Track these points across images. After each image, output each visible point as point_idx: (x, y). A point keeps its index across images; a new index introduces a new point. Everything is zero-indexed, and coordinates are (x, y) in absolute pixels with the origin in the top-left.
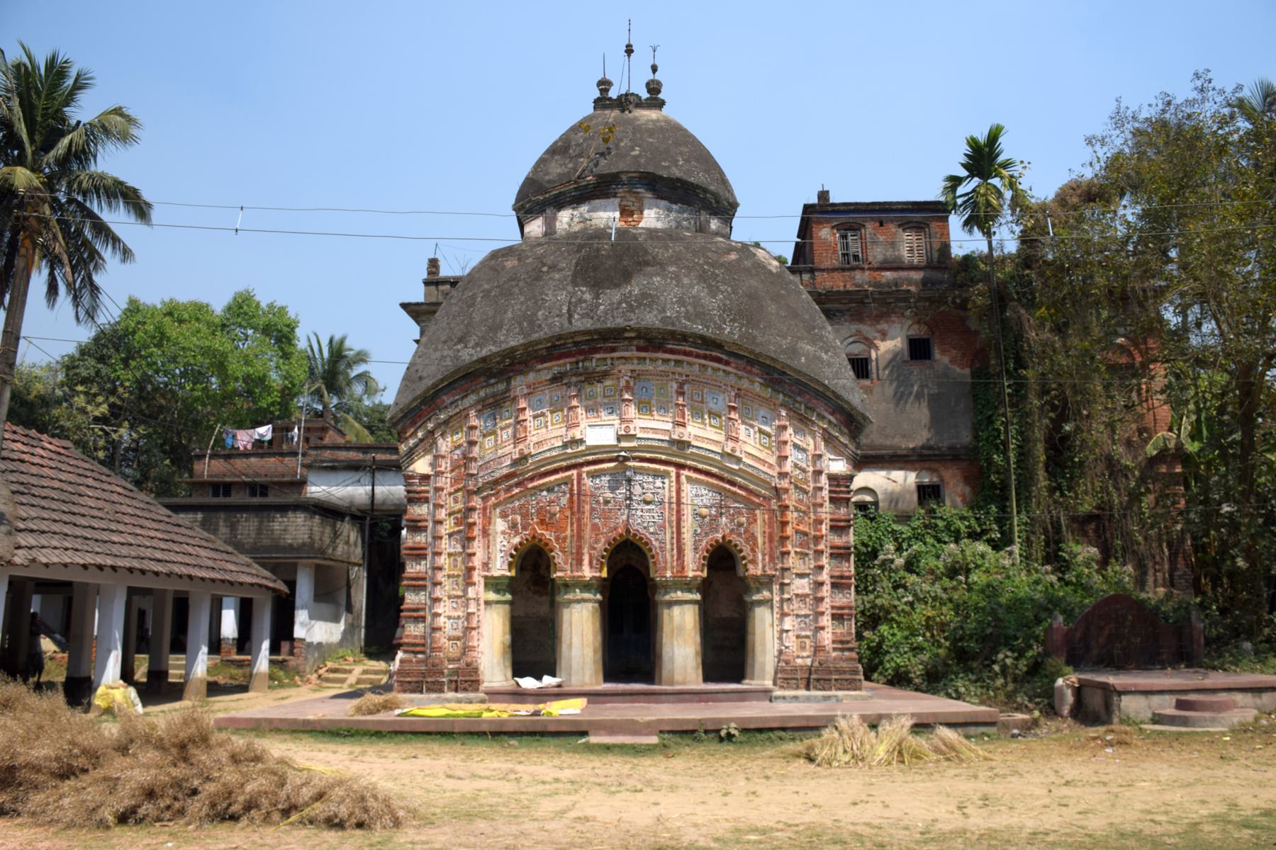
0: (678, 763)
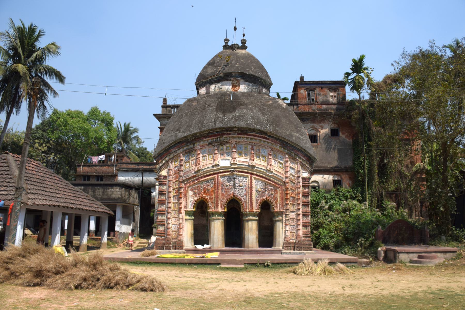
0: (251, 274)
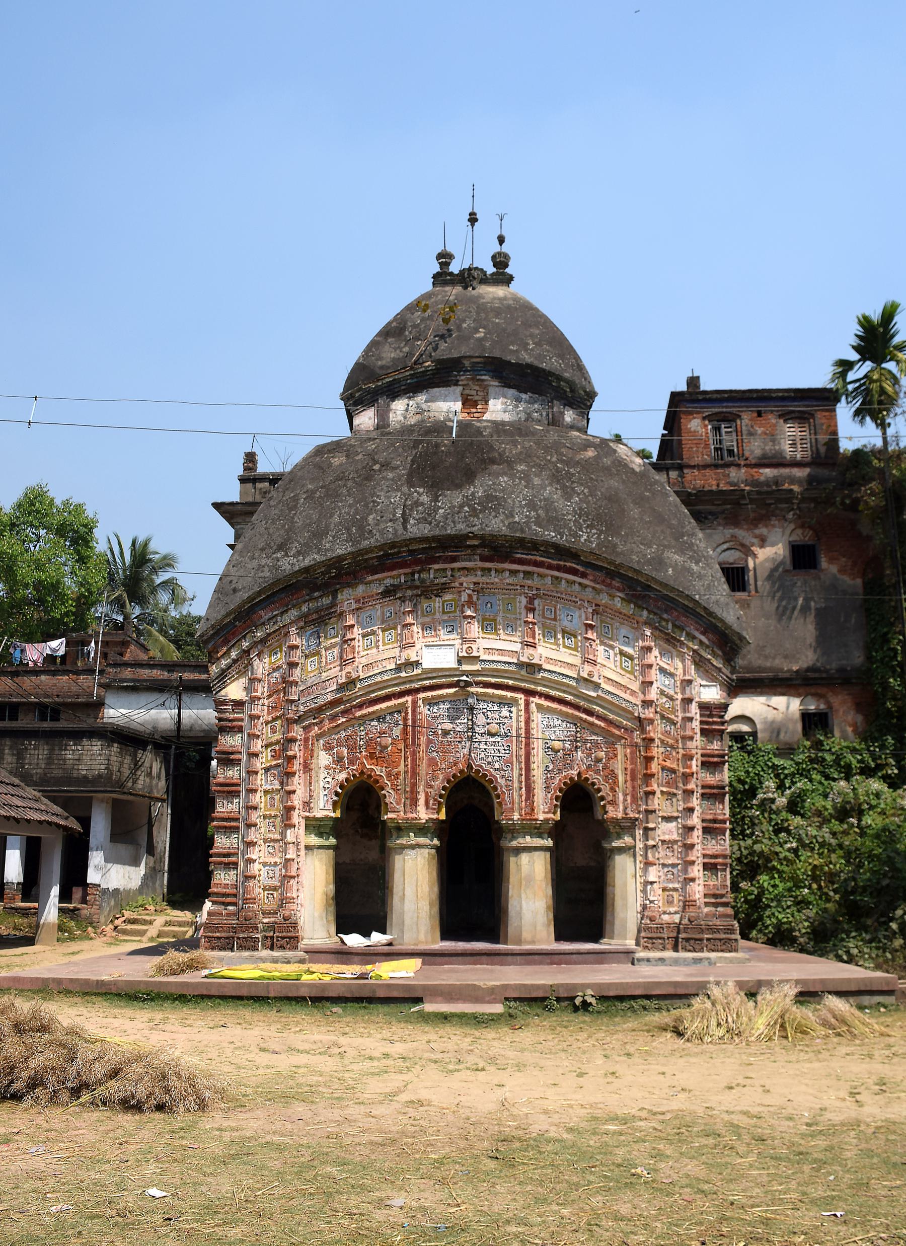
0: (526, 1037)
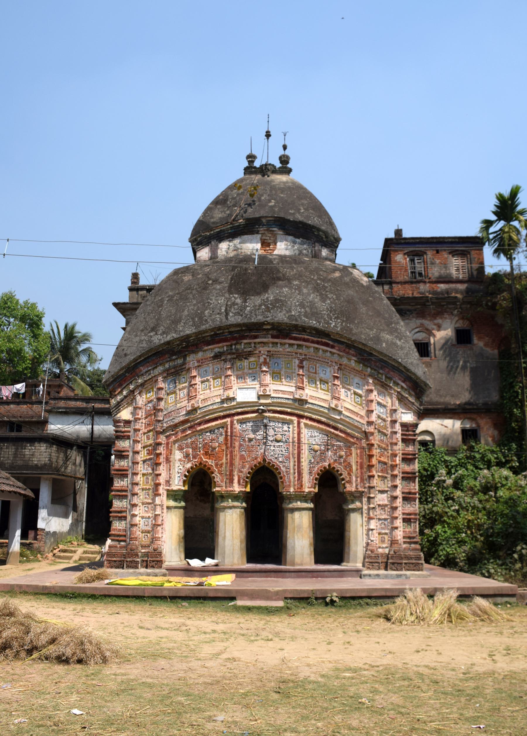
0: (297, 620)
